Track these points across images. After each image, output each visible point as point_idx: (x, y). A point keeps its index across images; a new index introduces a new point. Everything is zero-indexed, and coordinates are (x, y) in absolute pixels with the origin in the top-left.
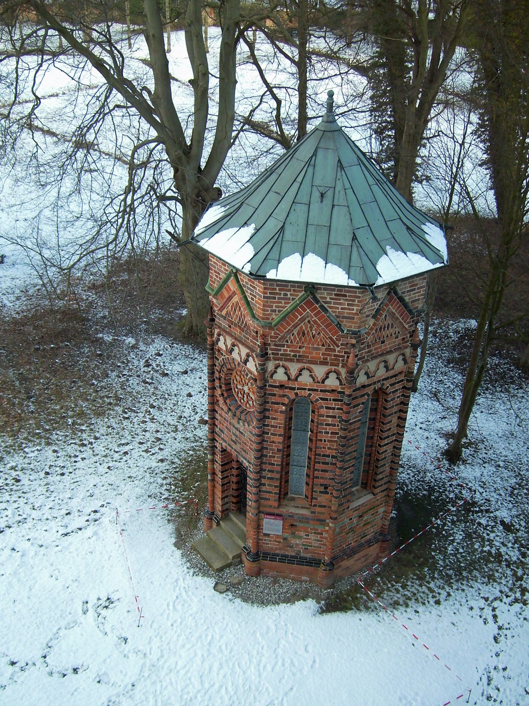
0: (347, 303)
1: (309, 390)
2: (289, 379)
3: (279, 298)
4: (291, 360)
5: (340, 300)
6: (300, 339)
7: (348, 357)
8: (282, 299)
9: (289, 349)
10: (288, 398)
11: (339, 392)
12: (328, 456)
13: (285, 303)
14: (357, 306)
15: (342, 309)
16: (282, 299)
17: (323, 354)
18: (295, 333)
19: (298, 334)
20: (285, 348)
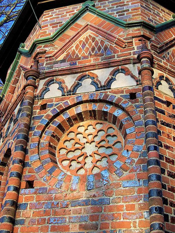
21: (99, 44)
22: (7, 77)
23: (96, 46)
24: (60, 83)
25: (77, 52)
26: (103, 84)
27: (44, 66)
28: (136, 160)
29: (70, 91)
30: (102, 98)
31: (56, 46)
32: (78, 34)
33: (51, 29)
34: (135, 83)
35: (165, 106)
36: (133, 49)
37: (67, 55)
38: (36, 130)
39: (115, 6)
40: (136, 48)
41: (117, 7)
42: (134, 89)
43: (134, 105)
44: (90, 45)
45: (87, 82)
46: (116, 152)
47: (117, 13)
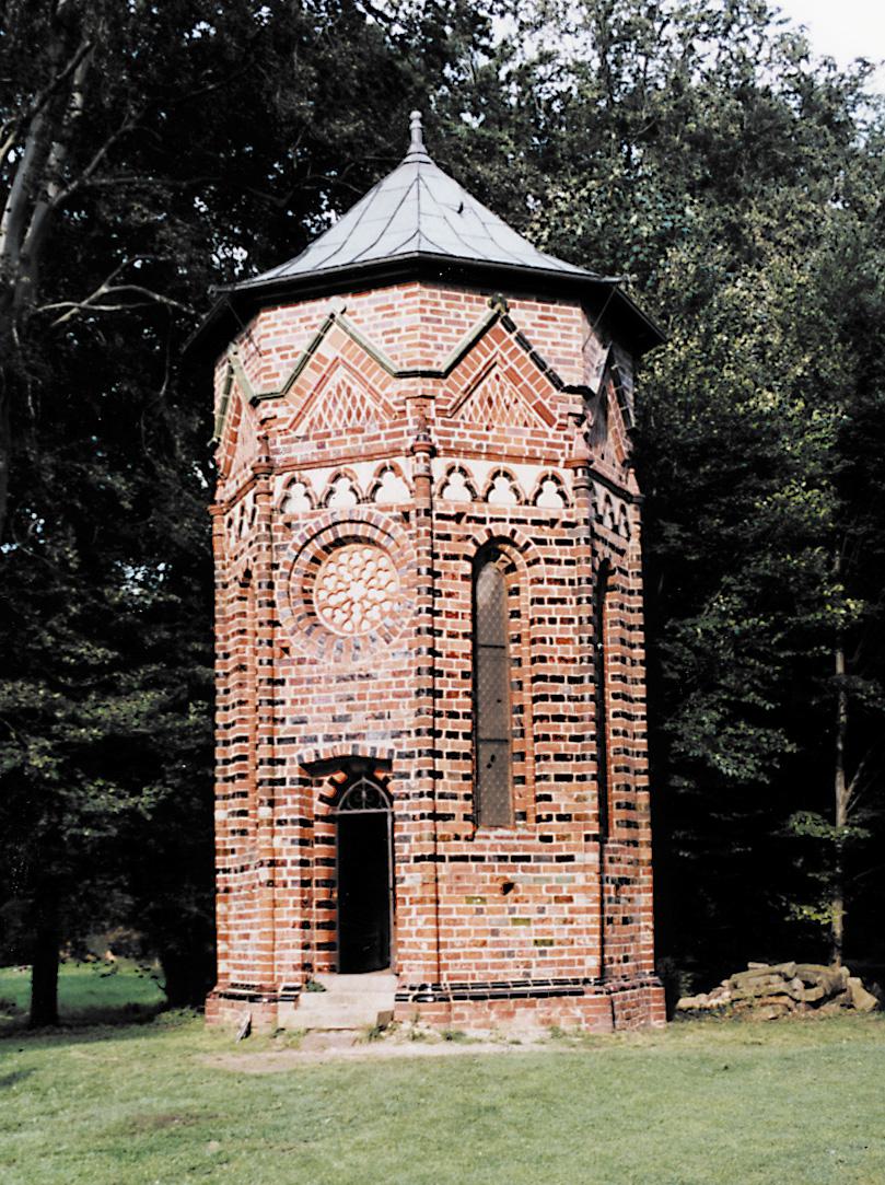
1: (512, 521)
2: (475, 498)
3: (447, 322)
4: (476, 454)
5: (546, 326)
6: (486, 413)
7: (571, 447)
8: (453, 323)
9: (468, 432)
10: (475, 542)
11: (566, 525)
12: (560, 679)
13: (459, 332)
14: (577, 338)
16: (453, 323)
17: (528, 442)
18: (476, 403)
19: (481, 402)
20: (462, 430)
22: (218, 404)
25: (325, 417)
30: (210, 1062)
31: (291, 406)
35: (453, 523)
39: (381, 313)
40: (411, 422)
42: (408, 506)
43: (406, 533)
44: (344, 403)
45: (342, 485)
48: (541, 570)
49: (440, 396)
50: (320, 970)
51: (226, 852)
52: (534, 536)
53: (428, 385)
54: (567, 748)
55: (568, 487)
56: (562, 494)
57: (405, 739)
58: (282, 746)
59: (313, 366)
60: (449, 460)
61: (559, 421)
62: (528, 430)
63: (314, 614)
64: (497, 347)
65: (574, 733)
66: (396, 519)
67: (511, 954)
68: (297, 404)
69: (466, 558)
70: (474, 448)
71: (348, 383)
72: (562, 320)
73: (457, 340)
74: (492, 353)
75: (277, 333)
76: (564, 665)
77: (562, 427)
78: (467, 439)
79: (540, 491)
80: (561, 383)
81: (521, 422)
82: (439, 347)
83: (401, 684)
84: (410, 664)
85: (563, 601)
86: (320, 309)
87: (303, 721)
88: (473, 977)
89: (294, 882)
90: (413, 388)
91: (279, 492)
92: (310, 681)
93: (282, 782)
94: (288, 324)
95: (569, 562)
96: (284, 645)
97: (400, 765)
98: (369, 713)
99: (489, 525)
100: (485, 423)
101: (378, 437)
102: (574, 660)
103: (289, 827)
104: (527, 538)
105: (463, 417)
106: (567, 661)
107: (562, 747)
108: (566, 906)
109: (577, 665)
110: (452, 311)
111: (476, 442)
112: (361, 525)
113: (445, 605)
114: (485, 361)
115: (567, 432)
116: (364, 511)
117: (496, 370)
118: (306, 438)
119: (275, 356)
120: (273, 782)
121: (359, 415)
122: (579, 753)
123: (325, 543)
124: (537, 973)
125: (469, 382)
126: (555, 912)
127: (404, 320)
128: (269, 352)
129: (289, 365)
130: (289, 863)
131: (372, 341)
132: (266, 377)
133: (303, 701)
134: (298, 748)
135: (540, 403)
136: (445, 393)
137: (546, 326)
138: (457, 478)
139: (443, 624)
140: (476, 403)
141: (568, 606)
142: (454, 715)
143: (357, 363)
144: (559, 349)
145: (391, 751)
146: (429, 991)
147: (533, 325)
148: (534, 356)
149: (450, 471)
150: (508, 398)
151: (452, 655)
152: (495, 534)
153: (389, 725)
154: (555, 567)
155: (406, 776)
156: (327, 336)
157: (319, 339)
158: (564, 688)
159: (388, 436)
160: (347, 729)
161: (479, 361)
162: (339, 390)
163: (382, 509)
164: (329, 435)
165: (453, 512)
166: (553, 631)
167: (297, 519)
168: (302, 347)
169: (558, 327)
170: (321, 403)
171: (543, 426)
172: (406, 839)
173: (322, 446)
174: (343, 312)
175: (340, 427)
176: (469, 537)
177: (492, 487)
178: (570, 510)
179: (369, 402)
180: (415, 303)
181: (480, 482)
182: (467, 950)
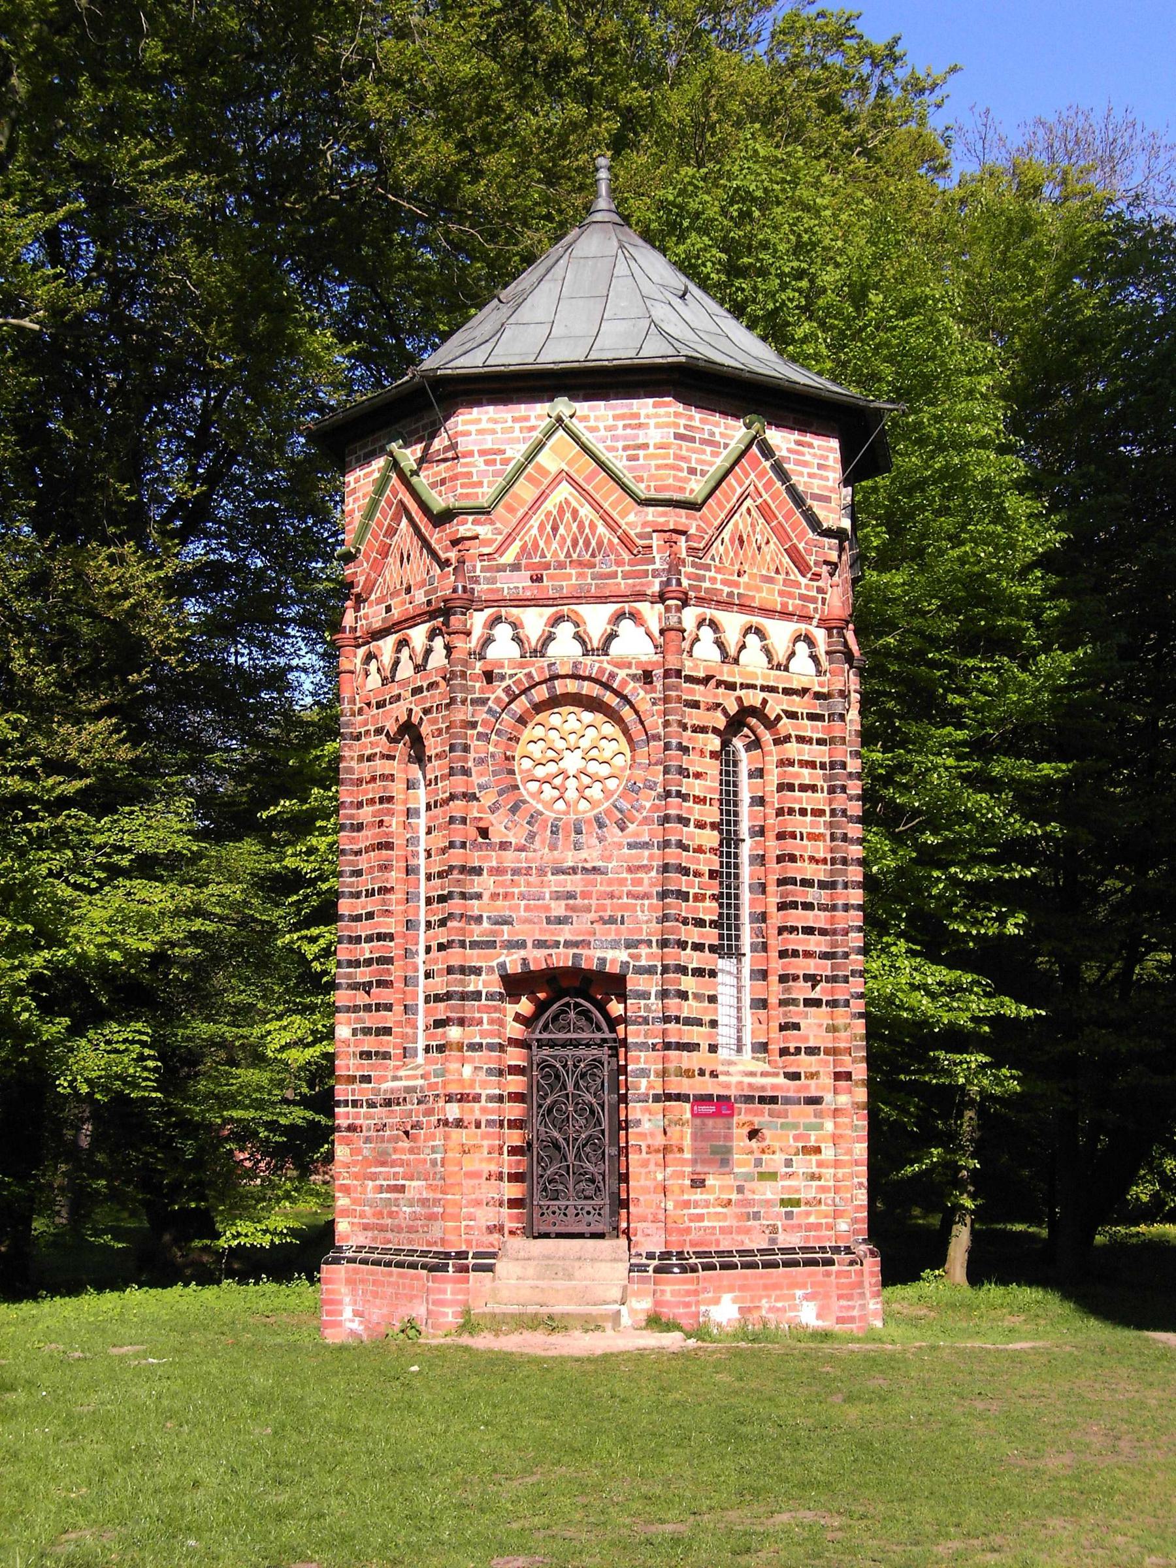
0: (816, 461)
1: (764, 688)
5: (803, 454)
6: (736, 554)
7: (824, 600)
9: (719, 577)
11: (818, 696)
15: (810, 475)
20: (712, 574)
21: (587, 530)
23: (581, 533)
24: (515, 626)
25: (542, 544)
26: (595, 645)
27: (478, 573)
28: (648, 805)
29: (535, 651)
31: (498, 525)
32: (542, 497)
33: (484, 467)
34: (653, 650)
35: (702, 688)
36: (652, 561)
37: (523, 548)
38: (479, 729)
39: (620, 424)
41: (625, 427)
42: (650, 663)
44: (568, 528)
46: (617, 772)
47: (625, 448)
48: (793, 750)
49: (692, 531)
50: (511, 1233)
51: (351, 1079)
52: (785, 707)
53: (678, 518)
54: (817, 967)
55: (821, 649)
56: (814, 658)
57: (644, 951)
58: (475, 952)
59: (530, 479)
60: (700, 610)
61: (814, 569)
62: (781, 577)
63: (516, 787)
64: (752, 476)
65: (824, 949)
66: (634, 677)
67: (756, 1217)
68: (505, 523)
69: (715, 731)
70: (724, 597)
71: (574, 504)
72: (820, 448)
73: (711, 464)
74: (747, 482)
75: (480, 432)
76: (814, 866)
77: (817, 576)
78: (718, 586)
79: (793, 654)
80: (819, 524)
81: (773, 568)
82: (692, 471)
83: (639, 882)
84: (651, 857)
85: (813, 788)
86: (538, 413)
87: (507, 922)
88: (718, 1243)
89: (489, 1123)
90: (662, 520)
91: (478, 631)
92: (516, 872)
93: (477, 995)
94: (496, 422)
95: (820, 742)
96: (481, 824)
97: (635, 983)
98: (593, 916)
99: (739, 693)
100: (736, 567)
101: (614, 575)
102: (824, 861)
103: (485, 1053)
104: (778, 710)
105: (713, 559)
106: (817, 862)
107: (811, 966)
108: (814, 1158)
109: (828, 867)
110: (707, 427)
111: (726, 589)
112: (586, 683)
113: (692, 786)
114: (739, 491)
115: (820, 583)
116: (592, 665)
117: (749, 503)
118: (515, 567)
119: (479, 461)
120: (464, 996)
121: (587, 544)
122: (829, 973)
123: (537, 699)
124: (786, 1239)
125: (723, 516)
126: (802, 1165)
127: (653, 436)
128: (470, 454)
129: (496, 474)
130: (483, 1098)
131: (610, 455)
132: (463, 486)
133: (506, 896)
134: (500, 955)
135: (794, 546)
136: (699, 528)
137: (803, 454)
138: (706, 633)
139: (690, 809)
140: (726, 540)
141: (819, 795)
142: (700, 923)
143: (589, 479)
144: (816, 482)
145: (625, 965)
146: (674, 1261)
147: (789, 450)
148: (792, 491)
149: (700, 625)
150: (759, 537)
151: (699, 850)
152: (746, 704)
153: (624, 932)
154: (807, 747)
155: (645, 995)
156: (550, 444)
157: (539, 447)
158: (813, 895)
159: (626, 576)
160: (566, 933)
161: (734, 491)
162: (561, 511)
163: (619, 665)
164: (547, 566)
165: (702, 675)
166: (804, 824)
167: (502, 667)
168: (517, 452)
169: (814, 455)
170: (536, 525)
171: (795, 575)
172: (644, 1073)
173: (538, 579)
174: (571, 417)
175: (562, 557)
176: (719, 705)
177: (743, 647)
178: (822, 679)
179: (601, 529)
180: (668, 415)
181: (732, 638)
182: (711, 1210)
